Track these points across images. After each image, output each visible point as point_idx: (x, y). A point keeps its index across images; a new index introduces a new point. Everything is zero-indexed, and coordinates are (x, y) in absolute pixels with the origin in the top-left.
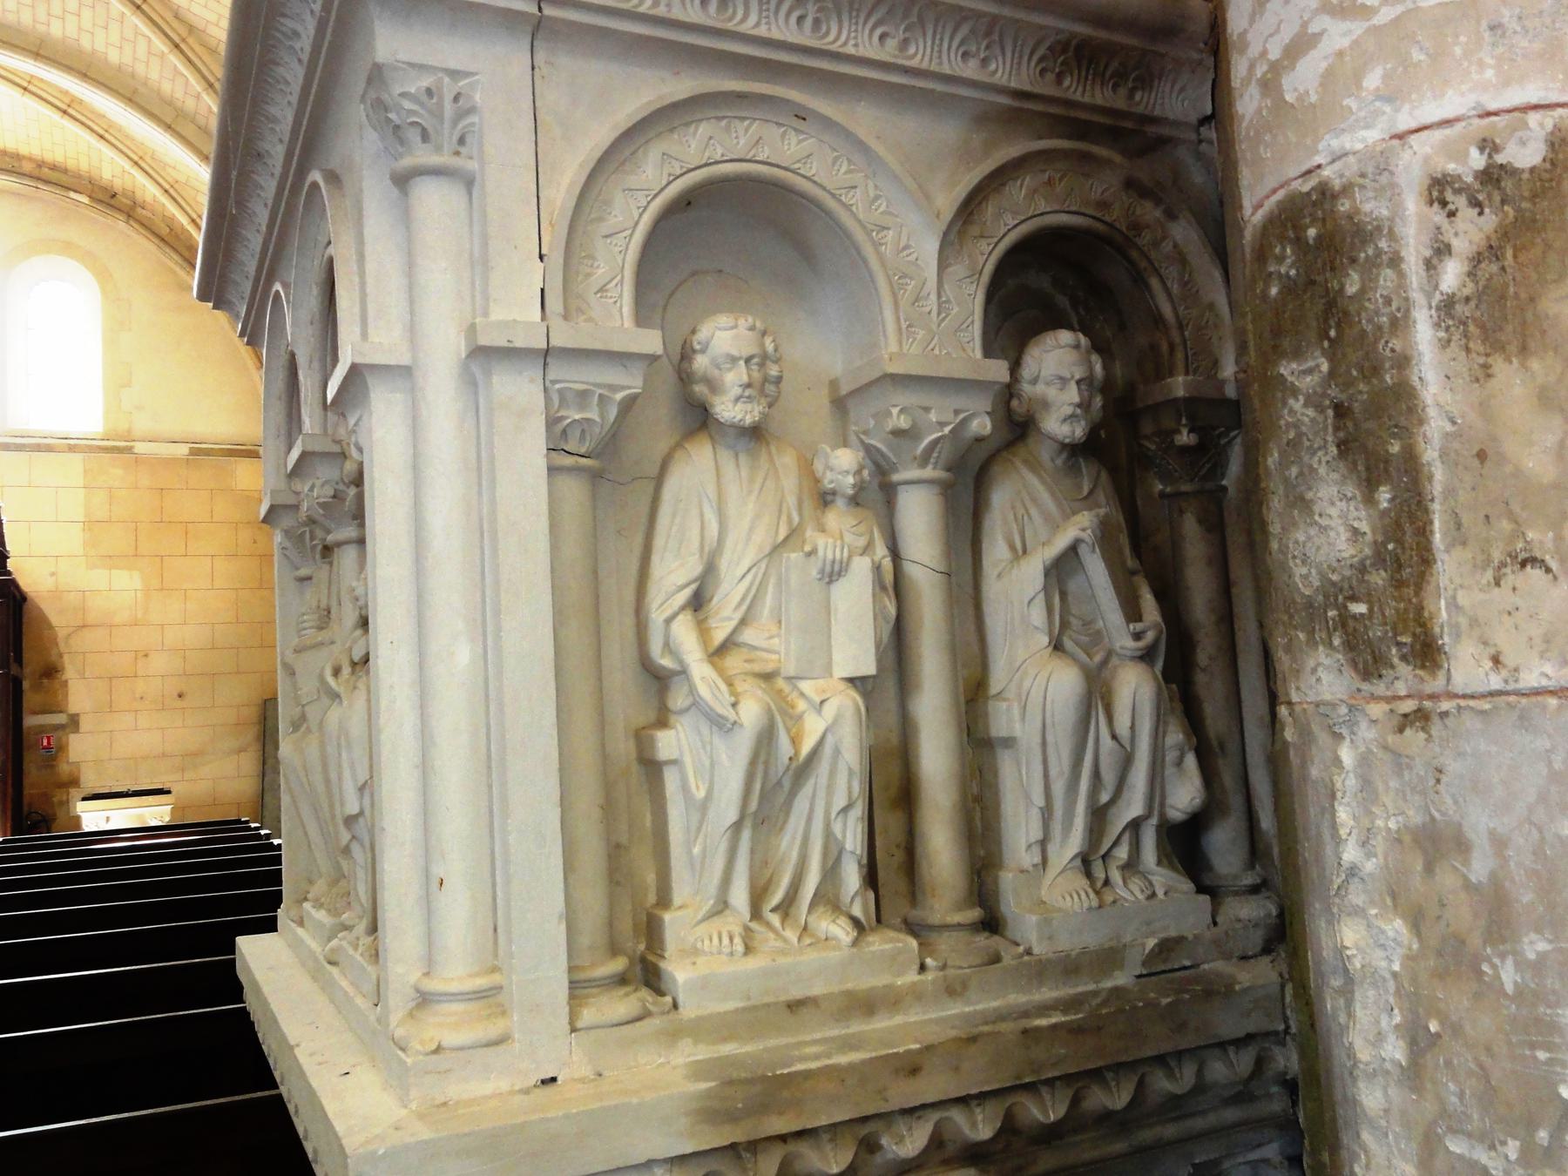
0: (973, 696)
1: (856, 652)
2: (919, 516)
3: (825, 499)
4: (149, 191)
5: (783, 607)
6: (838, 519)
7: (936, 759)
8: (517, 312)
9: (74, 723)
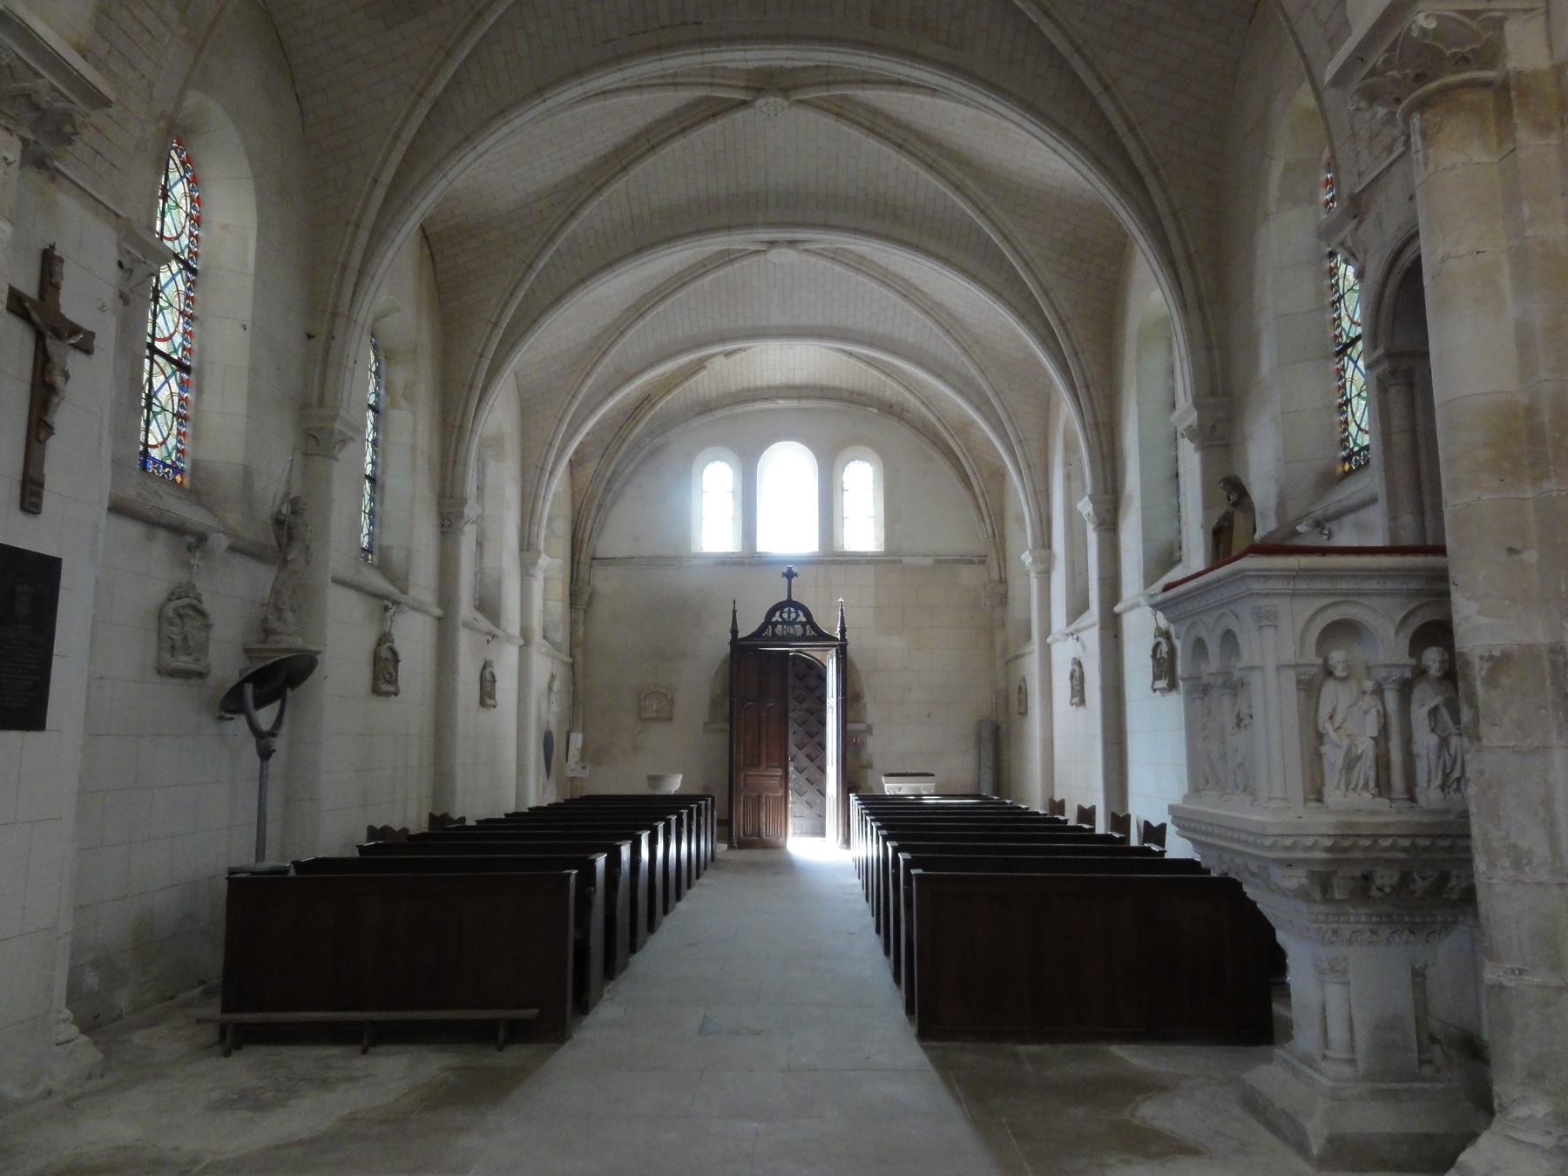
0: (1408, 741)
1: (1372, 729)
2: (1391, 699)
3: (1364, 693)
4: (913, 402)
5: (1353, 720)
6: (1367, 698)
7: (1396, 757)
8: (1289, 656)
9: (869, 730)
